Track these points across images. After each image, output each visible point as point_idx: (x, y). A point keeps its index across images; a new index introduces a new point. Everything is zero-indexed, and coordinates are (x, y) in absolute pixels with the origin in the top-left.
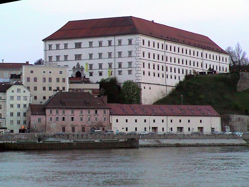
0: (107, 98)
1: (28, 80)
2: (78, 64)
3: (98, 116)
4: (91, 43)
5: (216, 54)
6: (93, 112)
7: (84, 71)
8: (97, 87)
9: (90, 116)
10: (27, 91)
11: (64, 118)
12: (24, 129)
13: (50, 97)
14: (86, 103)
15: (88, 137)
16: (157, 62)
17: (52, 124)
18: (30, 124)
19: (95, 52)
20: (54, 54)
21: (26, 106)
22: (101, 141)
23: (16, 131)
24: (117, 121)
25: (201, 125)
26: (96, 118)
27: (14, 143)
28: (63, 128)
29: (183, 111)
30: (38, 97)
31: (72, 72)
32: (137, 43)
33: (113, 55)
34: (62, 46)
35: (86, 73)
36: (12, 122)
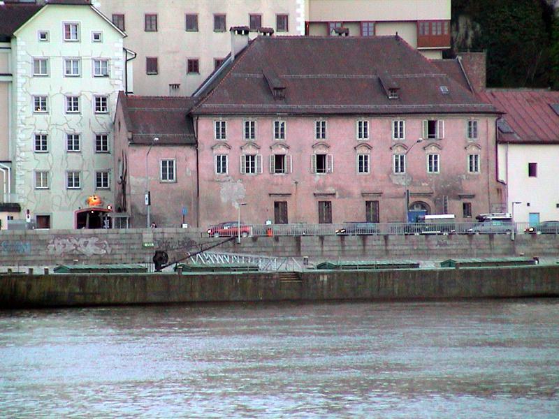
3: (439, 147)
6: (415, 128)
9: (404, 147)
10: (109, 35)
11: (279, 160)
12: (97, 212)
13: (218, 63)
14: (384, 89)
15: (390, 247)
17: (225, 188)
18: (124, 188)
21: (104, 104)
22: (449, 263)
23: (64, 220)
24: (532, 170)
26: (433, 159)
27: (43, 273)
28: (276, 204)
30: (162, 65)
36: (42, 178)
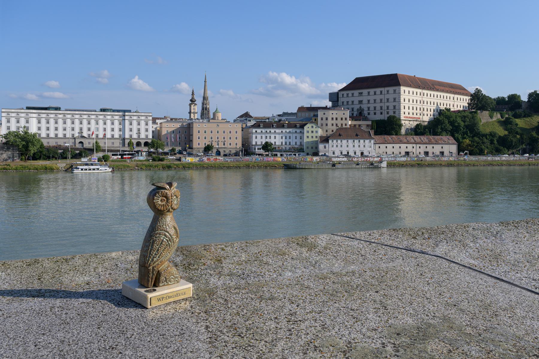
1: (322, 119)
2: (360, 107)
19: (372, 98)
24: (379, 147)
25: (442, 150)
33: (383, 101)
34: (350, 95)
35: (366, 113)
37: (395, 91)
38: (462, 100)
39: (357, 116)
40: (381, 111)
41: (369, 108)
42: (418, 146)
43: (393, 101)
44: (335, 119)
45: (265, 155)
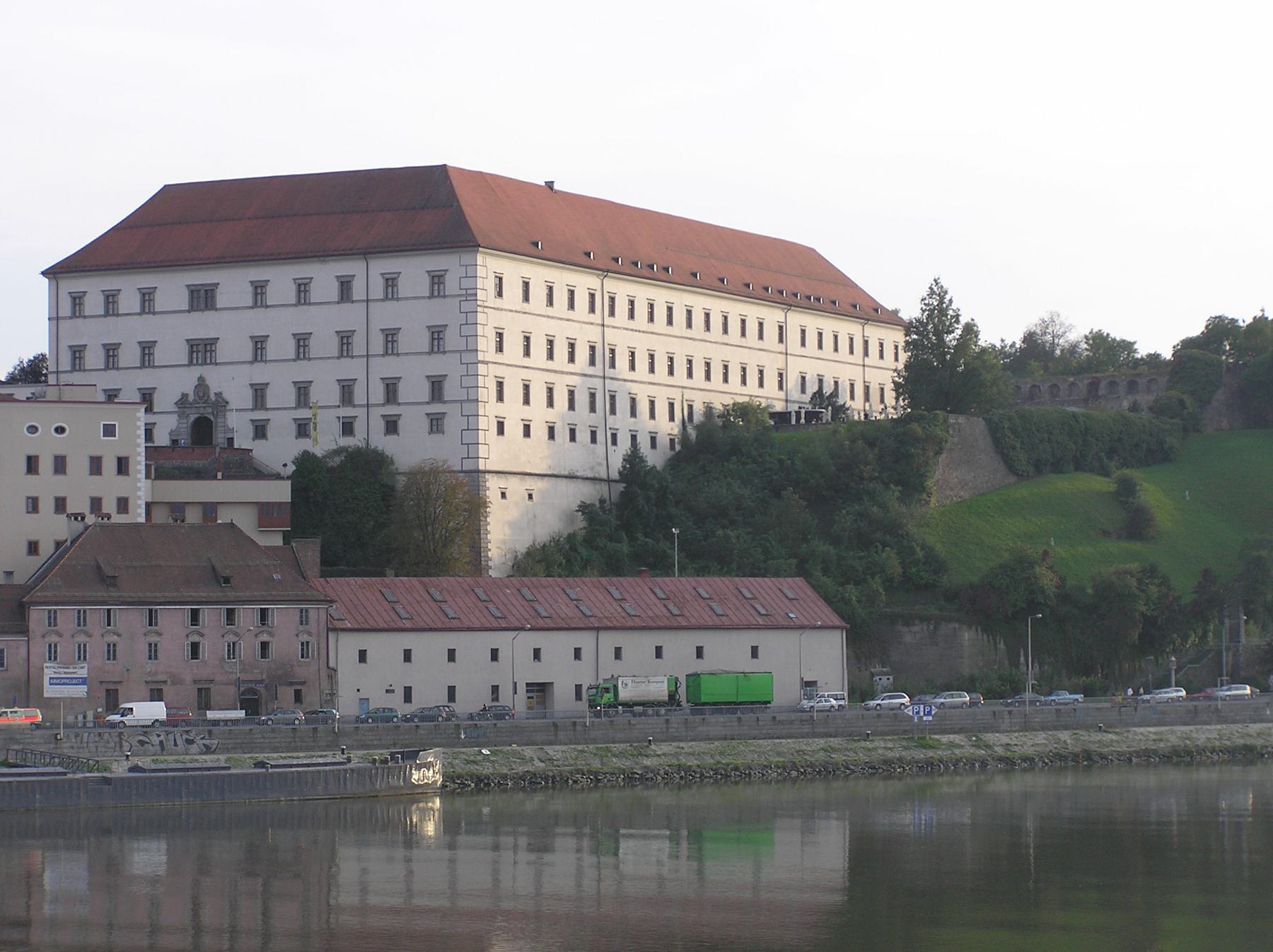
0: (318, 554)
2: (201, 385)
3: (270, 633)
4: (259, 289)
5: (846, 328)
7: (228, 414)
8: (281, 492)
13: (58, 544)
16: (562, 373)
20: (93, 334)
24: (363, 656)
29: (671, 607)
31: (175, 417)
32: (469, 292)
33: (358, 346)
34: (129, 302)
35: (238, 425)
37: (437, 279)
38: (641, 310)
39: (174, 442)
40: (347, 412)
41: (259, 393)
42: (609, 641)
43: (426, 348)
44: (46, 465)
45: (1201, 698)
